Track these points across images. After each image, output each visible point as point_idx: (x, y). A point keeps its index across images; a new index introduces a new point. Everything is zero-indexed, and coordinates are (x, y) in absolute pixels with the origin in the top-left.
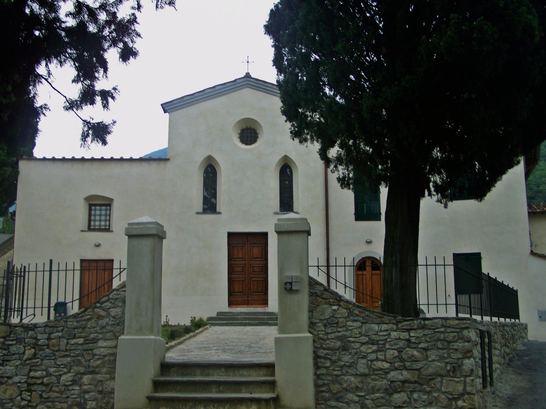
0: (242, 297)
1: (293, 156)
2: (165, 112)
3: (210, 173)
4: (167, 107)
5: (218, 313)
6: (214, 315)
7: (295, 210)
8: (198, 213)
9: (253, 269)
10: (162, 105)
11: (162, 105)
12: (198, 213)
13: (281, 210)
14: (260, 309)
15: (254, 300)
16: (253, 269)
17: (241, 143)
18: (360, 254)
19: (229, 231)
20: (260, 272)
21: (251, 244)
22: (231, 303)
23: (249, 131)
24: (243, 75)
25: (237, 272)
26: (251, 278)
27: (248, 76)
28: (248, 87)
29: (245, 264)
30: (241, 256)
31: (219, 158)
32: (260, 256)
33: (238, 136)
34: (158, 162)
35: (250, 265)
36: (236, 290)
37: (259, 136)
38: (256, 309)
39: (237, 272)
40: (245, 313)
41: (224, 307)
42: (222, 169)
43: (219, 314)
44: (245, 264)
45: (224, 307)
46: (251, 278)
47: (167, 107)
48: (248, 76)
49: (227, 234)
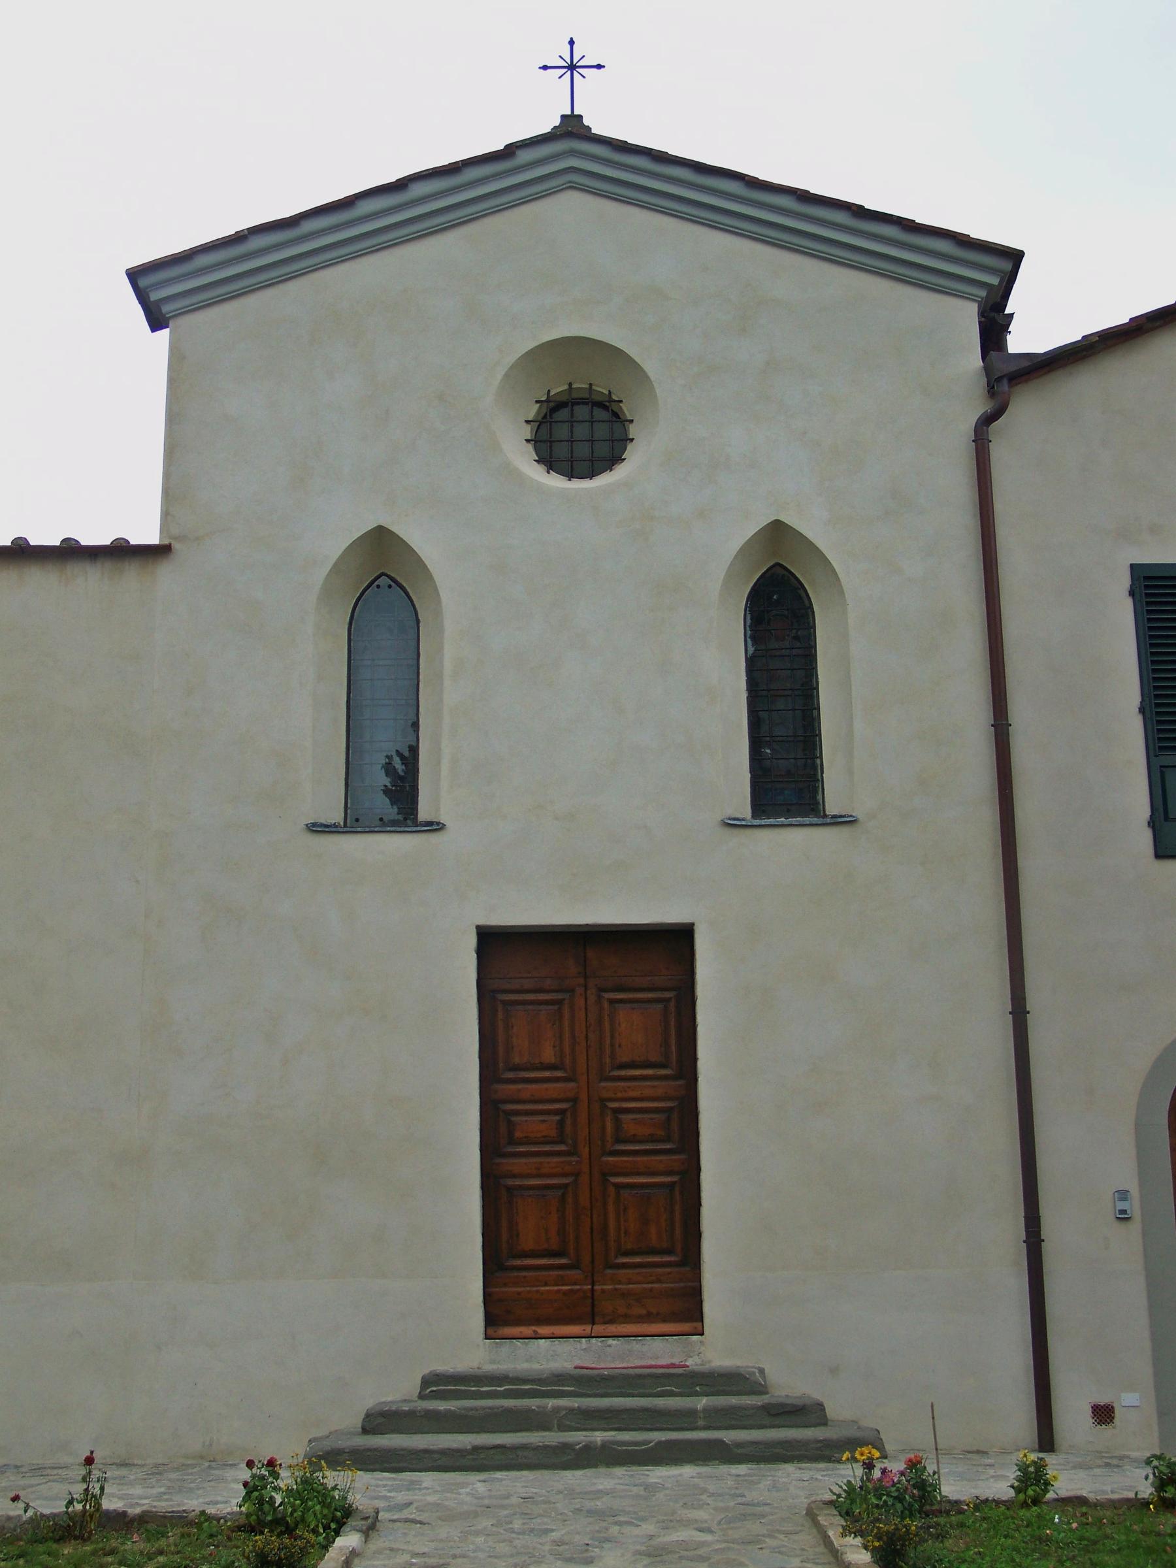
0: (560, 1281)
1: (811, 524)
2: (156, 322)
3: (383, 589)
4: (160, 289)
5: (426, 1382)
6: (400, 1389)
7: (832, 808)
8: (317, 828)
9: (618, 1123)
10: (134, 275)
11: (134, 275)
12: (317, 828)
13: (755, 815)
14: (658, 1351)
15: (624, 1295)
16: (618, 1123)
17: (541, 469)
18: (1139, 1128)
19: (483, 921)
20: (652, 1139)
21: (602, 990)
22: (499, 1317)
23: (582, 412)
24: (547, 122)
25: (528, 1141)
26: (604, 1175)
27: (572, 127)
28: (573, 187)
29: (575, 1100)
30: (548, 1054)
31: (421, 537)
32: (654, 1057)
33: (527, 432)
34: (108, 565)
35: (603, 1101)
36: (528, 1241)
37: (633, 431)
38: (635, 1345)
39: (528, 1141)
40: (586, 1381)
41: (468, 1347)
42: (449, 626)
43: (436, 1384)
44: (575, 1100)
45: (468, 1347)
46: (604, 1175)
47: (160, 289)
48: (572, 127)
49: (472, 941)
